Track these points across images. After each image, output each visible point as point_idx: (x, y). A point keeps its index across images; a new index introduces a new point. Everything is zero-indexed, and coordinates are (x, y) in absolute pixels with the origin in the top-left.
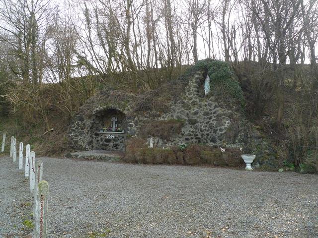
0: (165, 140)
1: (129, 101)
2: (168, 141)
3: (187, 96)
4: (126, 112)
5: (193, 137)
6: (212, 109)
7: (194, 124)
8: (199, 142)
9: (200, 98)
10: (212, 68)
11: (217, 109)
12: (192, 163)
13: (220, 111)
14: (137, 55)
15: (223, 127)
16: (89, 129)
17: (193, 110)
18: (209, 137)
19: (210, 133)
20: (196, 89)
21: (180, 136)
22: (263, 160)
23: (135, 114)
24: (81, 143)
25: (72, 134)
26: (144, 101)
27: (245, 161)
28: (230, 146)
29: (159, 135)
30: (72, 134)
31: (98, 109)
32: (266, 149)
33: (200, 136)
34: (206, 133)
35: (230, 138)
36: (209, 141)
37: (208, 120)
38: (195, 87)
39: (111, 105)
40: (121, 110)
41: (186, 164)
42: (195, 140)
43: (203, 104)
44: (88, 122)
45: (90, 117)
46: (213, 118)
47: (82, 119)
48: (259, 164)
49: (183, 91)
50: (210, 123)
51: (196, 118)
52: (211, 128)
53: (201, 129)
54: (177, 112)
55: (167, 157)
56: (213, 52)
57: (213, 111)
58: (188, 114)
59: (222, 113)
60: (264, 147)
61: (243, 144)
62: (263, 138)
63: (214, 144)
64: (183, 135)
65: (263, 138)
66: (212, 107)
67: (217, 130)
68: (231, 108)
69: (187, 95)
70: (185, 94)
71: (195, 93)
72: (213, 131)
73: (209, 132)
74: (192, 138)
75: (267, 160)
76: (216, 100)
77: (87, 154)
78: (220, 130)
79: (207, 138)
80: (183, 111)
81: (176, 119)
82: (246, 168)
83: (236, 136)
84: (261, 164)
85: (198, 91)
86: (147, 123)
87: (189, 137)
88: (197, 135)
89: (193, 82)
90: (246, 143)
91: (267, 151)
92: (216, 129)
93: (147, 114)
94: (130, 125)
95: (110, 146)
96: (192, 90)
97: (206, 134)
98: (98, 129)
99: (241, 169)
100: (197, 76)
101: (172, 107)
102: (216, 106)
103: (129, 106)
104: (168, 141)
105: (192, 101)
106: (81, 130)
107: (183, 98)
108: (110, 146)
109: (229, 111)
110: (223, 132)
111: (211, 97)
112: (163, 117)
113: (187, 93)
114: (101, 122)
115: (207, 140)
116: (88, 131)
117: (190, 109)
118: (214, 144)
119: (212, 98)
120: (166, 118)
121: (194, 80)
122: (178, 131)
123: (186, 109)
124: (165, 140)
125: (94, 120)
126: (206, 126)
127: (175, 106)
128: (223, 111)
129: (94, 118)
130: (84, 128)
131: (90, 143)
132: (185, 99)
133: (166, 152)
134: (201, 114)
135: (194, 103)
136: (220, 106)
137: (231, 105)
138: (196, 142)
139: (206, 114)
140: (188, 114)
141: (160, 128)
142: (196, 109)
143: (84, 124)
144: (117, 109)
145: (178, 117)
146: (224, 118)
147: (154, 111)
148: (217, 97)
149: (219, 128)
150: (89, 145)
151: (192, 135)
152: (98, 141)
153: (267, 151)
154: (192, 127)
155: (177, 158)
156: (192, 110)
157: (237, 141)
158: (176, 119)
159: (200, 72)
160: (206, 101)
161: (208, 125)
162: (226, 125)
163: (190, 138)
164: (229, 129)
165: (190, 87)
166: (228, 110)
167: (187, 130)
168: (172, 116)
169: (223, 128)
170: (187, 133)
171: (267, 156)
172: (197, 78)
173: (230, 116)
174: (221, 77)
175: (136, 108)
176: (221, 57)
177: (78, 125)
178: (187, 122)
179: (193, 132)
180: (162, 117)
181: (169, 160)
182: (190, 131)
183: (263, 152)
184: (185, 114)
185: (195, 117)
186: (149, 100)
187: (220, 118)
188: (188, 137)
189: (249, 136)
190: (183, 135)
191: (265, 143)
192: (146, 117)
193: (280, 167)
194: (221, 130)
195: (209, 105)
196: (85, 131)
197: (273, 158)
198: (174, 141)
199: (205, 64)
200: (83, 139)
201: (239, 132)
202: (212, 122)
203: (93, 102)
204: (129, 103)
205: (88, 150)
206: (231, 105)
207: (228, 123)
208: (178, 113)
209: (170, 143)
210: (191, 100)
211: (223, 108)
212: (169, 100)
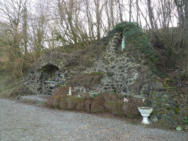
0: (88, 89)
1: (62, 59)
2: (90, 89)
3: (107, 54)
4: (59, 67)
5: (110, 86)
6: (125, 63)
7: (111, 76)
8: (115, 91)
9: (117, 55)
10: (125, 29)
11: (129, 63)
12: (95, 111)
13: (131, 65)
14: (91, 26)
15: (132, 79)
16: (38, 79)
17: (111, 65)
18: (122, 87)
19: (123, 83)
20: (115, 48)
21: (100, 85)
22: (161, 114)
23: (65, 68)
24: (31, 89)
25: (26, 83)
26: (74, 58)
27: (142, 114)
28: (136, 96)
29: (83, 84)
30: (26, 83)
31: (43, 65)
32: (166, 102)
33: (116, 87)
34: (120, 83)
35: (136, 89)
36: (122, 91)
37: (122, 73)
38: (114, 46)
39: (51, 62)
40: (57, 65)
41: (90, 112)
42: (112, 90)
43: (119, 59)
44: (38, 75)
45: (39, 70)
46: (126, 71)
47: (33, 72)
48: (157, 117)
49: (104, 49)
50: (123, 75)
51: (113, 71)
52: (124, 80)
53: (116, 80)
54: (99, 66)
55: (76, 104)
56: (132, 17)
57: (125, 65)
58: (107, 68)
59: (132, 66)
60: (164, 100)
61: (146, 95)
62: (164, 90)
63: (125, 94)
64: (102, 85)
65: (164, 90)
66: (125, 62)
67: (127, 82)
68: (140, 62)
69: (107, 52)
70: (106, 51)
71: (113, 51)
72: (125, 83)
73: (122, 83)
74: (109, 88)
75: (165, 115)
76: (128, 56)
77: (32, 98)
78: (130, 81)
79: (120, 88)
80: (103, 65)
81: (98, 72)
82: (142, 122)
83: (141, 87)
84: (159, 118)
85: (116, 49)
86: (75, 75)
87: (107, 87)
88: (113, 85)
89: (112, 42)
90: (148, 95)
91: (167, 105)
92: (127, 80)
93: (76, 68)
94: (61, 76)
95: (52, 92)
96: (112, 48)
97: (120, 85)
98: (47, 79)
99: (134, 123)
100: (115, 37)
101: (95, 63)
102: (128, 61)
103: (62, 63)
104: (90, 89)
105: (110, 57)
106: (32, 80)
107: (103, 55)
108: (52, 92)
109: (138, 65)
110: (132, 83)
111: (125, 54)
112: (88, 71)
113: (108, 51)
114: (50, 75)
115: (120, 90)
116: (38, 81)
117: (109, 63)
118: (125, 94)
119: (125, 54)
120: (89, 71)
121: (113, 40)
122: (99, 81)
123: (106, 64)
124: (88, 89)
125: (42, 73)
126: (120, 78)
127: (97, 61)
128: (133, 65)
129: (42, 71)
130: (35, 79)
131: (40, 89)
132: (105, 55)
133: (76, 100)
134: (117, 67)
135: (112, 59)
136: (131, 60)
137: (140, 59)
138: (112, 91)
139: (121, 68)
140: (107, 68)
141: (84, 79)
142: (114, 64)
143: (34, 76)
144: (54, 64)
145: (99, 70)
146: (133, 71)
147: (81, 66)
148: (128, 52)
149: (129, 80)
150: (38, 91)
151: (109, 85)
152: (46, 88)
153: (167, 105)
154: (110, 79)
155: (84, 106)
156: (110, 64)
157: (141, 92)
158: (98, 72)
159: (117, 34)
160: (121, 57)
161: (121, 77)
162: (135, 77)
163: (108, 88)
164: (137, 80)
165: (109, 46)
166: (137, 63)
167: (106, 81)
168: (95, 70)
169: (132, 80)
170: (106, 83)
171: (166, 110)
172: (115, 39)
173: (139, 69)
174: (132, 35)
175: (67, 63)
176: (128, 21)
177: (30, 77)
178: (106, 75)
179: (110, 82)
180: (87, 71)
181: (78, 107)
182: (108, 82)
183: (163, 105)
184: (105, 68)
185: (113, 71)
186: (77, 57)
187: (130, 71)
188: (106, 87)
189: (151, 88)
190: (102, 85)
191: (166, 96)
192: (75, 71)
193: (179, 124)
194: (130, 81)
195: (123, 60)
196: (36, 80)
197: (173, 112)
198: (95, 89)
199: (121, 26)
200: (34, 86)
201: (144, 83)
202: (124, 74)
203: (41, 60)
204: (62, 60)
205: (36, 95)
206: (140, 59)
207: (137, 75)
208: (99, 67)
209: (92, 92)
210: (109, 56)
211: (133, 62)
212: (93, 57)
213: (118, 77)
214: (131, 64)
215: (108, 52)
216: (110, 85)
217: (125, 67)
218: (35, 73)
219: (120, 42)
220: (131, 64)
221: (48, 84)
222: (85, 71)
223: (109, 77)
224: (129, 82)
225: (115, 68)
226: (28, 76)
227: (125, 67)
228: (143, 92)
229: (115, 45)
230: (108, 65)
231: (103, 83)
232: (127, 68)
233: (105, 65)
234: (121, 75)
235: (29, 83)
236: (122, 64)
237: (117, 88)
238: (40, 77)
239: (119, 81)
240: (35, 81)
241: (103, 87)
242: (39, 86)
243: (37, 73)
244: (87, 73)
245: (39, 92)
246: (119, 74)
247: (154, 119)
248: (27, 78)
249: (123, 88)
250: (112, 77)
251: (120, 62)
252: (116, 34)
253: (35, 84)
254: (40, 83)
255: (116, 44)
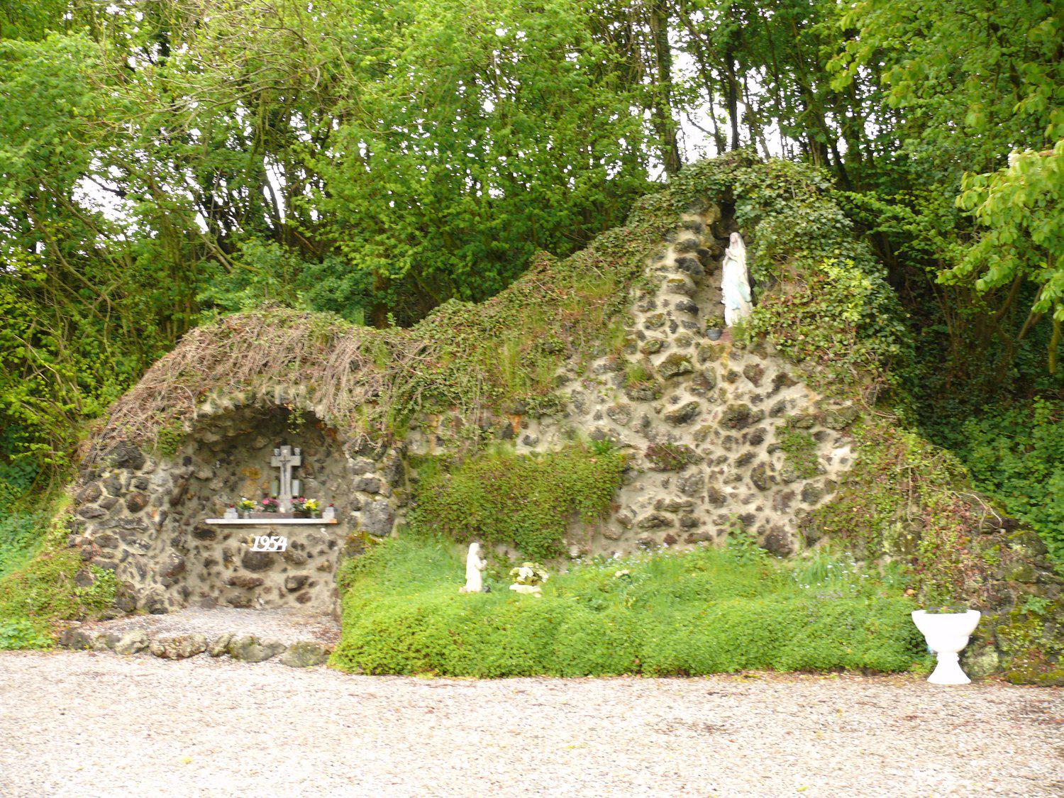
16: (166, 507)
21: (614, 528)
25: (87, 535)
37: (746, 448)
43: (721, 372)
44: (160, 476)
46: (770, 439)
50: (756, 462)
57: (768, 405)
71: (679, 317)
85: (693, 310)
95: (268, 590)
96: (666, 304)
100: (686, 236)
108: (268, 590)
112: (527, 442)
117: (656, 395)
120: (542, 443)
129: (190, 451)
130: (146, 503)
140: (647, 424)
154: (673, 487)
156: (665, 400)
159: (697, 218)
169: (820, 485)
172: (686, 248)
179: (675, 508)
180: (519, 441)
185: (685, 438)
190: (624, 523)
196: (152, 515)
200: (144, 560)
207: (843, 461)
208: (598, 417)
213: (722, 472)
214: (806, 396)
215: (647, 328)
216: (677, 524)
217: (767, 413)
218: (148, 466)
219: (711, 260)
220: (806, 396)
221: (226, 538)
222: (507, 446)
223: (663, 477)
224: (800, 497)
225: (699, 419)
226: (101, 485)
227: (767, 413)
228: (896, 544)
229: (688, 281)
230: (655, 404)
231: (630, 515)
232: (780, 422)
233: (633, 404)
234: (744, 461)
235: (109, 533)
236: (746, 397)
237: (716, 540)
238: (176, 491)
239: (733, 496)
240: (146, 522)
241: (630, 534)
242: (169, 556)
243: (156, 464)
244: (524, 458)
245: (176, 595)
246: (726, 459)
247: (980, 659)
248: (94, 499)
249: (760, 533)
250: (687, 474)
251: (730, 388)
252: (686, 218)
253: (145, 539)
254: (174, 535)
255: (691, 276)
